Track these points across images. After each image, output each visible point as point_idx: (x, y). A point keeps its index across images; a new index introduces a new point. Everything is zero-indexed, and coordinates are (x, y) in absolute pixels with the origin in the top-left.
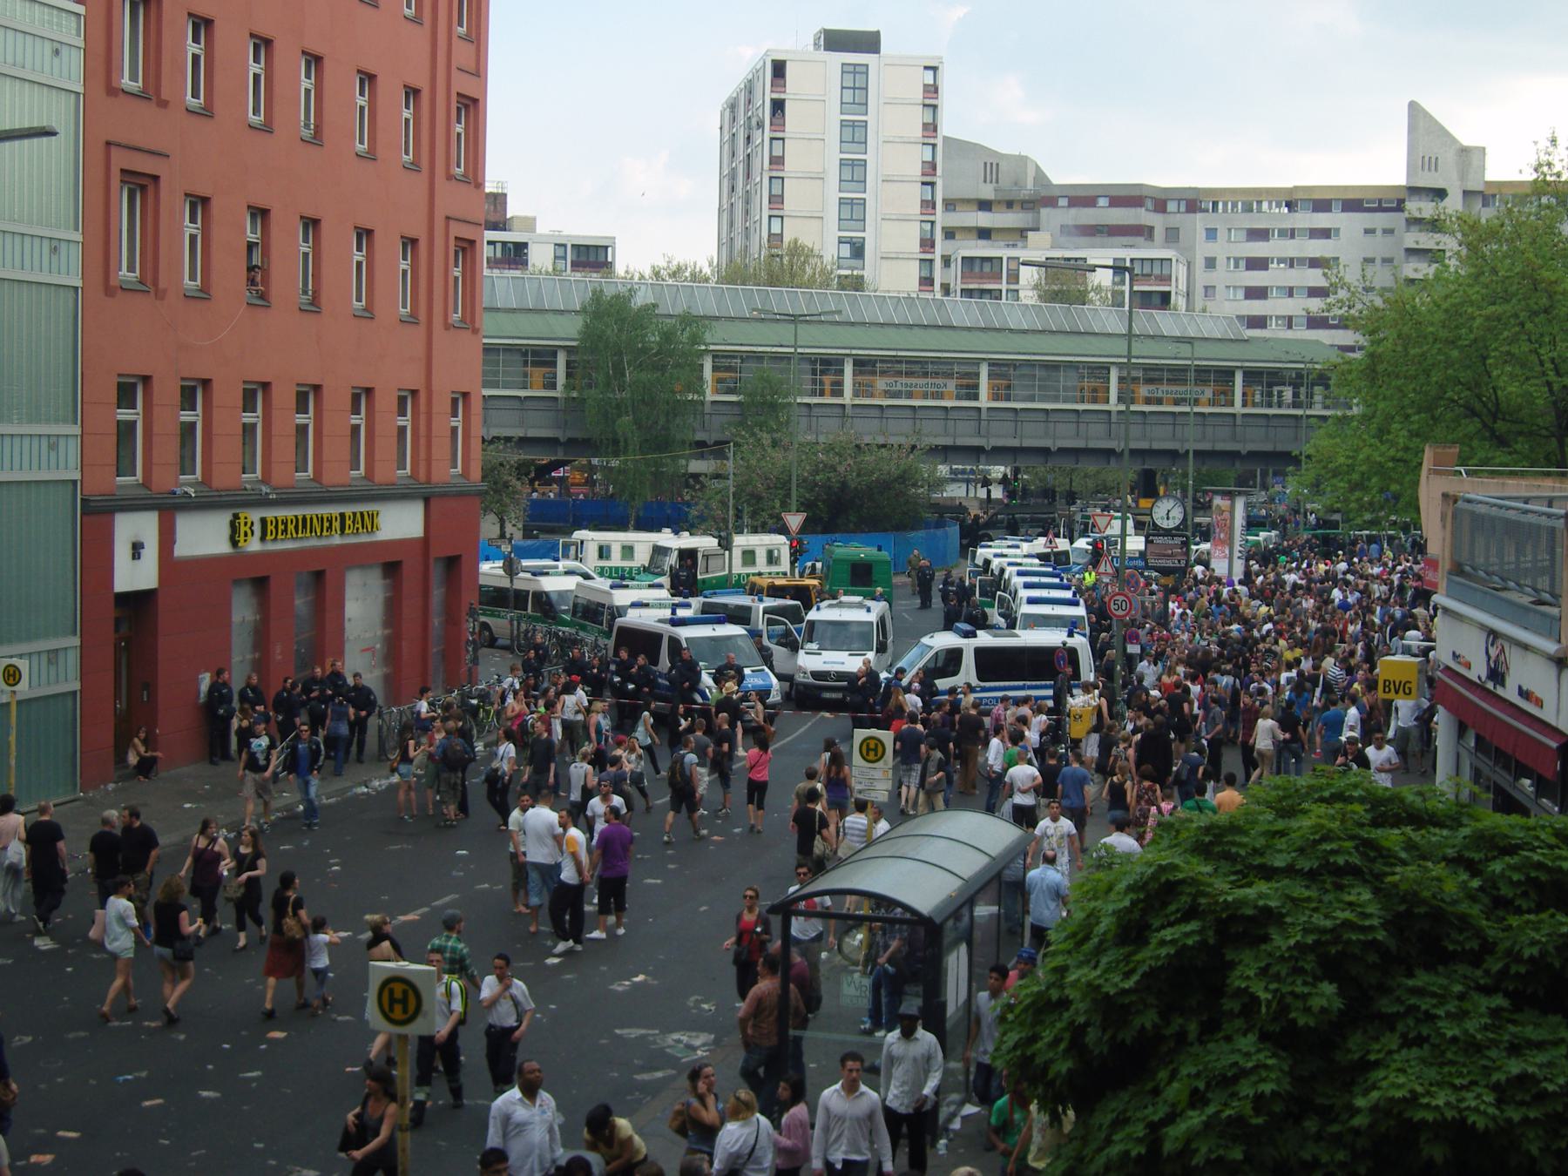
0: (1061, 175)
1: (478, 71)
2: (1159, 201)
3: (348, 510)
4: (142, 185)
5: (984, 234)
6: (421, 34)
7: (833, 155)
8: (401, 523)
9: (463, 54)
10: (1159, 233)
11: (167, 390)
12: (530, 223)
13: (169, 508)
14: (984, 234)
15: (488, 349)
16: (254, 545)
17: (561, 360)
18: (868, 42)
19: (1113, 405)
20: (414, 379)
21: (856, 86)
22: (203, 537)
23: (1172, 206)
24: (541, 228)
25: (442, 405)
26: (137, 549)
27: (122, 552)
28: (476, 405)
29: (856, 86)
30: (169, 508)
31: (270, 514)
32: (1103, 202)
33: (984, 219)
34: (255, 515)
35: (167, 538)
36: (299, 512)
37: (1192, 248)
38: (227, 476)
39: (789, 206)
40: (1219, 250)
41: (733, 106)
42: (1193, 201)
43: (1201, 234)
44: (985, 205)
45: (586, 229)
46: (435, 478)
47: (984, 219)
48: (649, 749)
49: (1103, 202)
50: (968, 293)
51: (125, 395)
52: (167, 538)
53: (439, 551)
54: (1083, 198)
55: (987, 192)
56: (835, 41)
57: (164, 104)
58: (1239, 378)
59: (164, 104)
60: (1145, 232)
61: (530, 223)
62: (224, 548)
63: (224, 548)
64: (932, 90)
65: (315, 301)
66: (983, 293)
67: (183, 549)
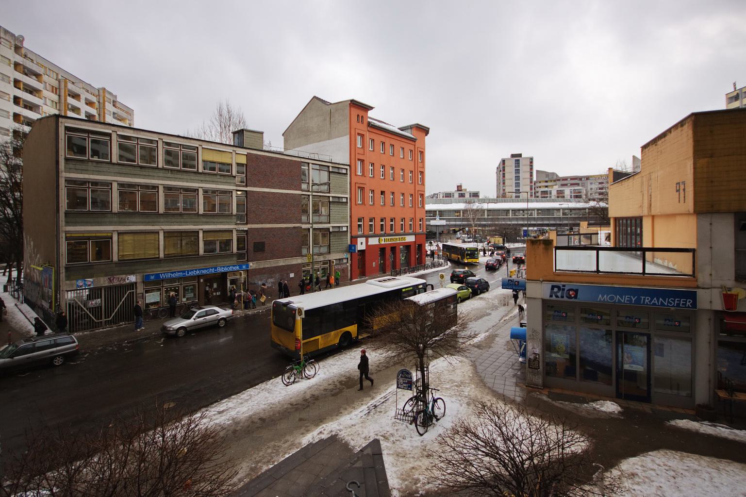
0: (561, 175)
1: (423, 167)
2: (580, 178)
3: (400, 237)
4: (362, 189)
5: (546, 187)
6: (413, 163)
7: (514, 175)
8: (410, 239)
9: (420, 165)
10: (580, 184)
11: (367, 219)
12: (466, 190)
13: (367, 237)
14: (546, 187)
15: (426, 211)
16: (383, 243)
17: (461, 212)
18: (520, 155)
19: (486, 217)
20: (413, 217)
21: (517, 162)
22: (373, 241)
23: (583, 179)
24: (467, 190)
25: (418, 220)
26: (362, 243)
27: (359, 243)
28: (424, 220)
29: (517, 162)
30: (367, 237)
31: (386, 238)
32: (569, 179)
33: (546, 184)
34: (383, 238)
35: (367, 242)
36: (391, 237)
37: (587, 187)
38: (378, 232)
39: (506, 184)
40: (594, 186)
41: (498, 168)
42: (588, 178)
43: (589, 184)
44: (546, 182)
45: (474, 190)
46: (417, 231)
47: (546, 184)
48: (146, 281)
49: (569, 179)
50: (543, 197)
51: (382, 220)
52: (367, 242)
53: (418, 243)
54: (565, 179)
55: (547, 179)
56: (513, 156)
57: (365, 176)
58: (511, 211)
59: (365, 176)
60: (578, 184)
61: (466, 190)
62: (378, 243)
63: (378, 243)
64: (531, 162)
65: (394, 205)
66: (545, 197)
67: (369, 244)
